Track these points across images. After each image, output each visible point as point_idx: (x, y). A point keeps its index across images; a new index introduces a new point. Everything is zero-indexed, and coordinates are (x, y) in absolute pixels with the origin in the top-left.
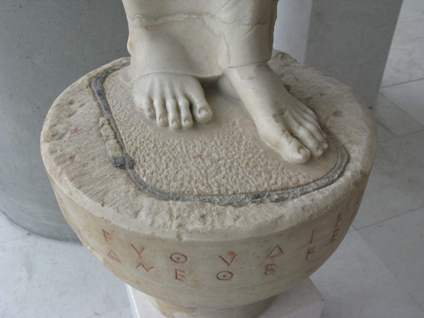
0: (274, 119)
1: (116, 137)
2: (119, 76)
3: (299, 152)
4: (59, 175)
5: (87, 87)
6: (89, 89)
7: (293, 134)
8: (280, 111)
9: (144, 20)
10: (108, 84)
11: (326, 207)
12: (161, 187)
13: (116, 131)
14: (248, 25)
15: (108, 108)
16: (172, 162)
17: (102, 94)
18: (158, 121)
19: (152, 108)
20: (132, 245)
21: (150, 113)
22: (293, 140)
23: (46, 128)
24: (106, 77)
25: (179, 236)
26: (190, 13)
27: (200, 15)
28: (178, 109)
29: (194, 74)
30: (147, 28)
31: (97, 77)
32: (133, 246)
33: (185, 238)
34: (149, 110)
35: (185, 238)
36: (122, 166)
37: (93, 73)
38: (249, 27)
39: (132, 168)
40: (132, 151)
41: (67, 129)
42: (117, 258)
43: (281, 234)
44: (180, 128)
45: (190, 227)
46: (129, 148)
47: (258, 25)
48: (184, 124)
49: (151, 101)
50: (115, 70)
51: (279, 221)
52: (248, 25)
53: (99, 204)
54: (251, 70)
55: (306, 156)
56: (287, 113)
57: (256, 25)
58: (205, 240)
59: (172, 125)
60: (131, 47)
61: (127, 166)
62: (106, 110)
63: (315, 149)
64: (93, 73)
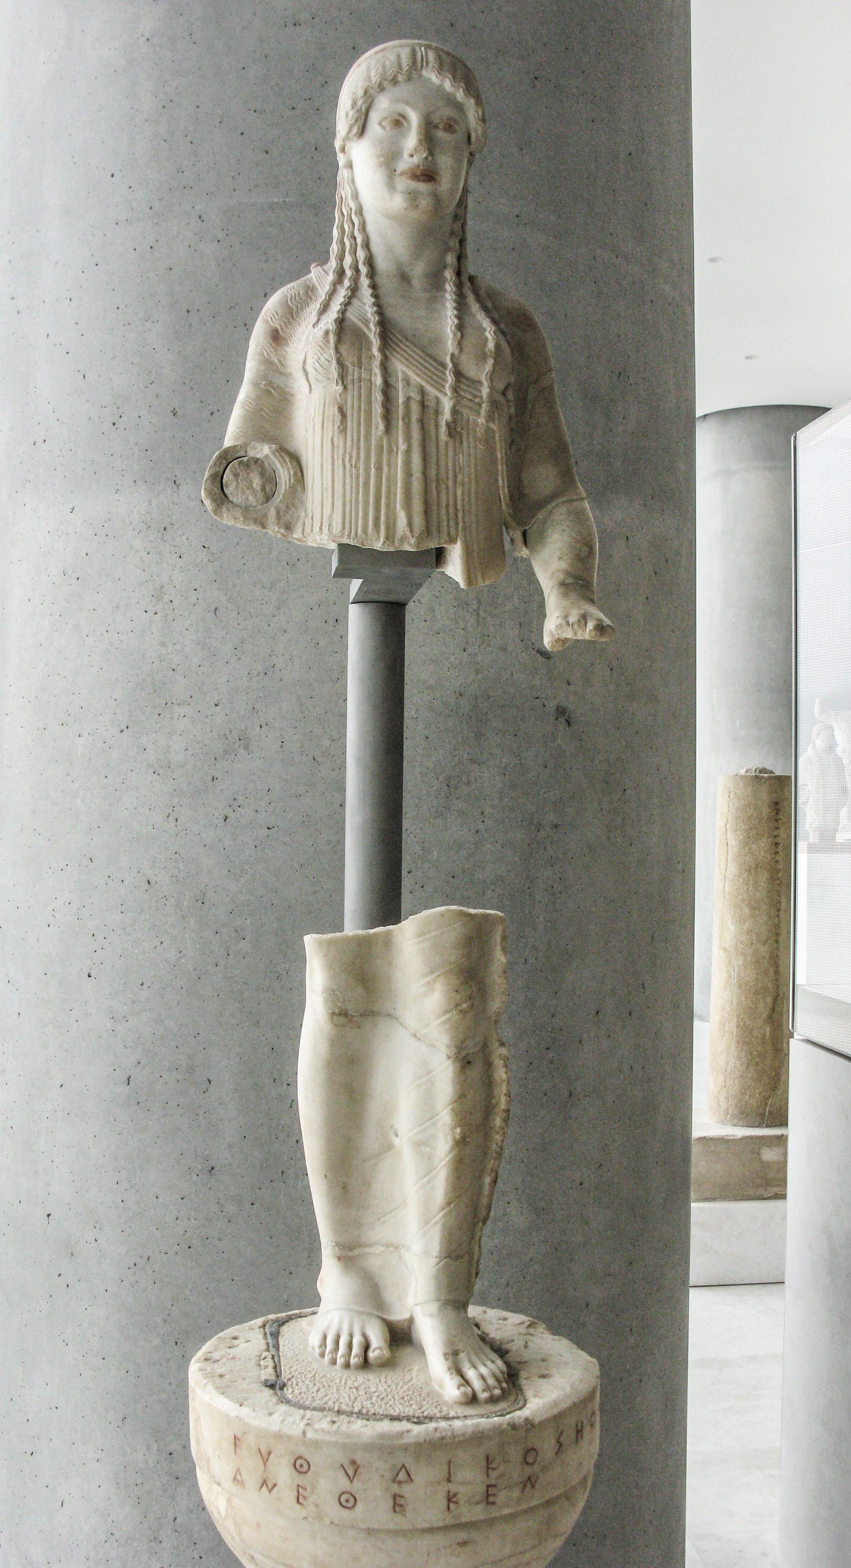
0: (444, 1357)
1: (275, 1367)
2: (303, 1322)
3: (458, 1388)
4: (204, 1386)
5: (259, 1328)
6: (262, 1329)
7: (460, 1373)
8: (454, 1351)
9: (337, 1249)
10: (285, 1329)
11: (463, 1435)
12: (304, 1402)
13: (277, 1363)
14: (436, 1257)
15: (277, 1347)
16: (325, 1389)
17: (276, 1335)
18: (328, 1357)
19: (324, 1343)
20: (259, 1449)
21: (320, 1349)
22: (456, 1378)
23: (204, 1349)
24: (288, 1321)
25: (304, 1433)
26: (388, 1246)
27: (396, 1247)
28: (350, 1346)
29: (380, 1314)
30: (339, 1259)
31: (274, 1321)
32: (260, 1452)
33: (310, 1435)
34: (320, 1346)
35: (310, 1435)
36: (272, 1387)
37: (272, 1316)
38: (435, 1261)
39: (282, 1388)
40: (288, 1377)
41: (223, 1357)
42: (242, 1481)
43: (405, 1448)
44: (347, 1365)
45: (316, 1426)
46: (285, 1376)
47: (448, 1259)
48: (353, 1361)
49: (325, 1337)
50: (301, 1317)
51: (405, 1434)
52: (436, 1257)
53: (238, 1405)
54: (434, 1307)
55: (465, 1394)
56: (462, 1355)
57: (445, 1258)
58: (328, 1438)
59: (340, 1361)
60: (321, 1282)
61: (277, 1387)
62: (274, 1347)
63: (481, 1390)
64: (272, 1316)
